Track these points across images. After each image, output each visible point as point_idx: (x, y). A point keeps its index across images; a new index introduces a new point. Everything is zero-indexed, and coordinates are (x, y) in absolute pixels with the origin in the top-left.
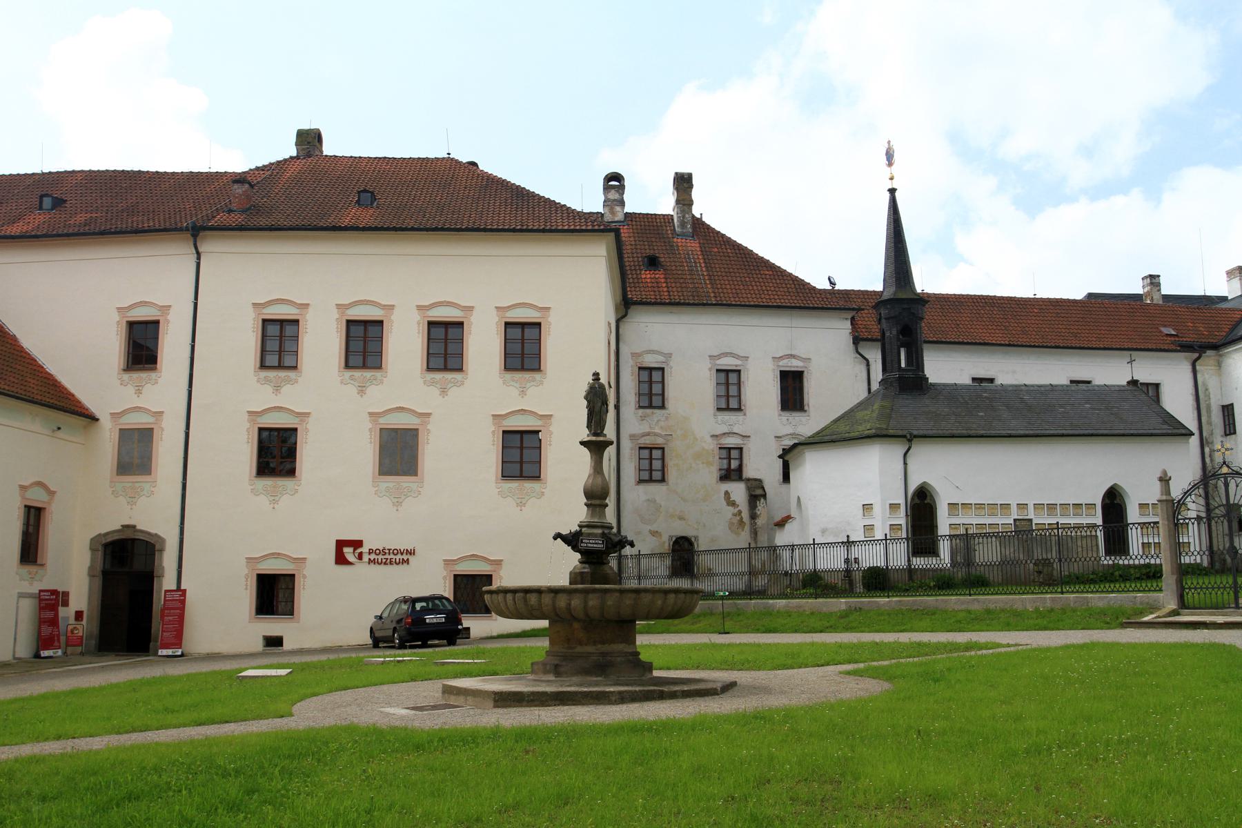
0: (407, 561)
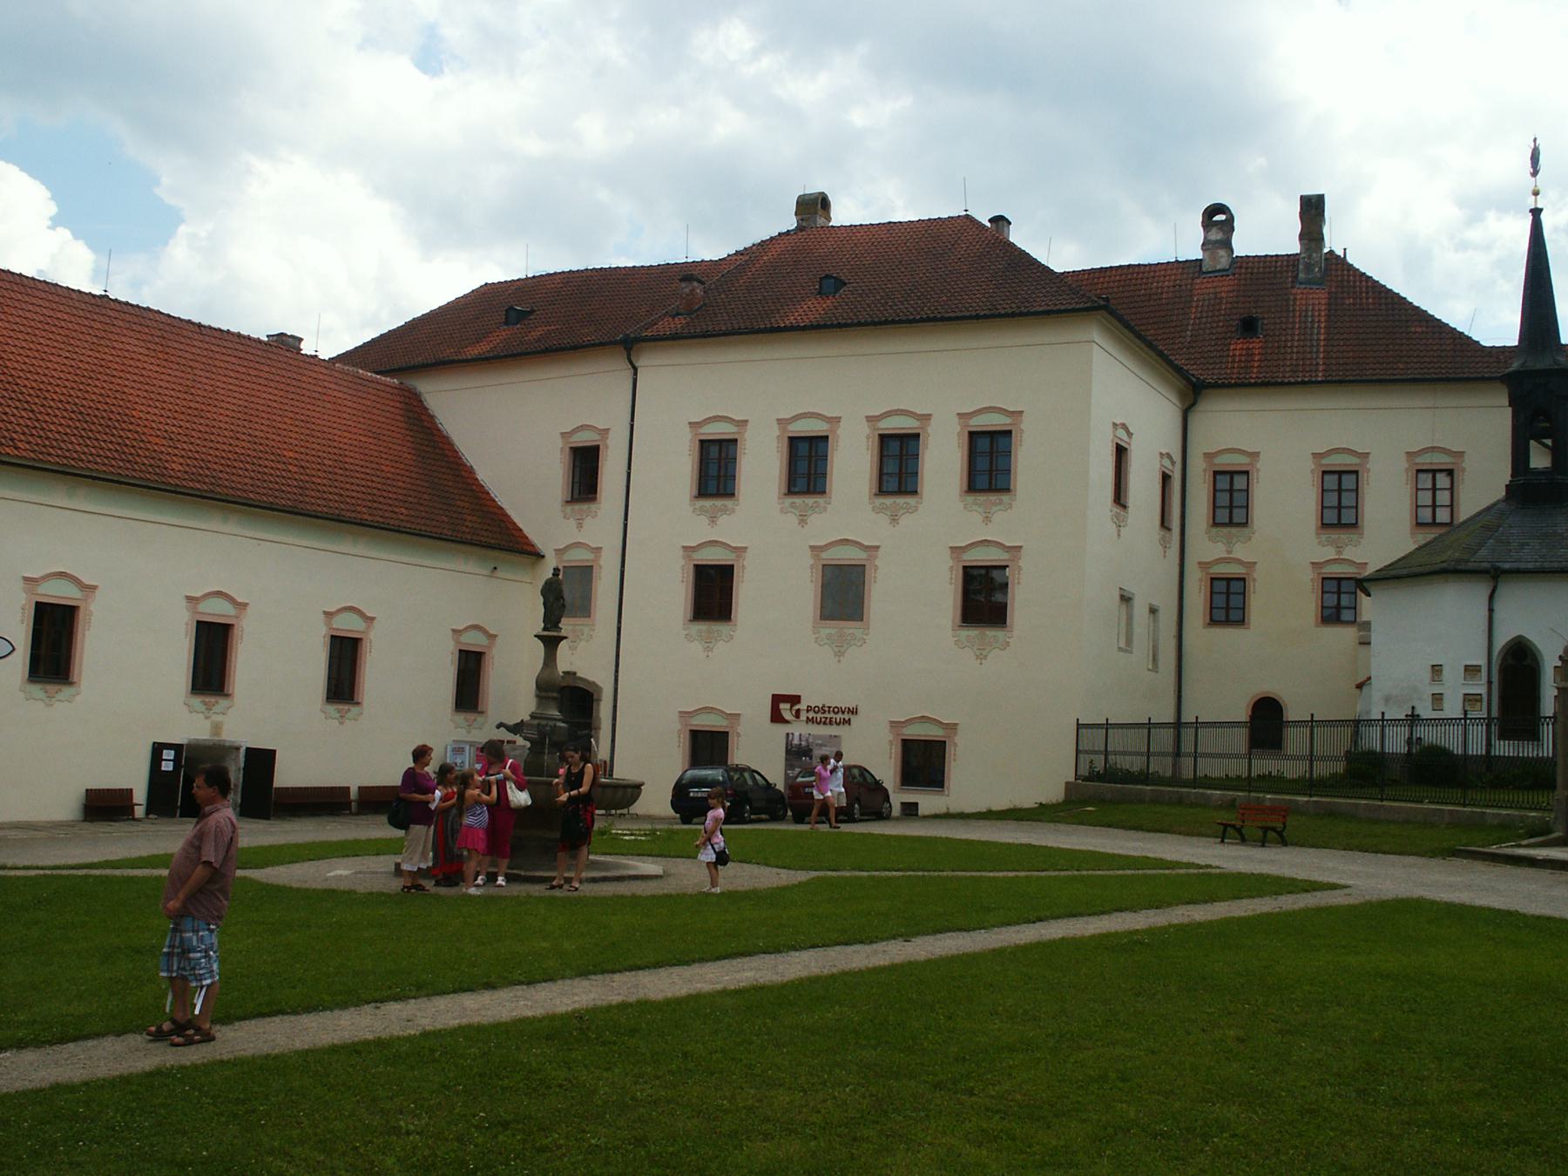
0: (849, 722)
